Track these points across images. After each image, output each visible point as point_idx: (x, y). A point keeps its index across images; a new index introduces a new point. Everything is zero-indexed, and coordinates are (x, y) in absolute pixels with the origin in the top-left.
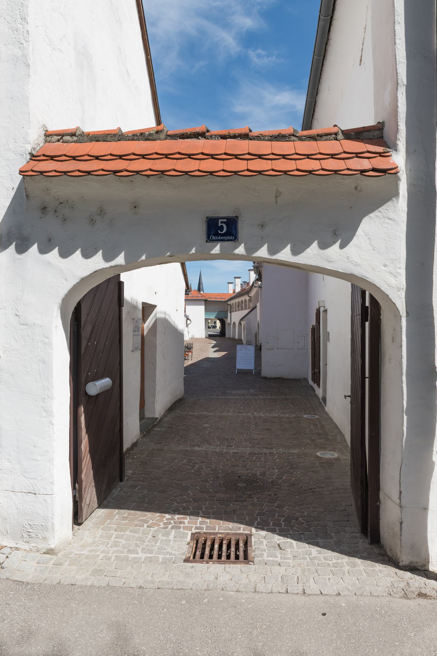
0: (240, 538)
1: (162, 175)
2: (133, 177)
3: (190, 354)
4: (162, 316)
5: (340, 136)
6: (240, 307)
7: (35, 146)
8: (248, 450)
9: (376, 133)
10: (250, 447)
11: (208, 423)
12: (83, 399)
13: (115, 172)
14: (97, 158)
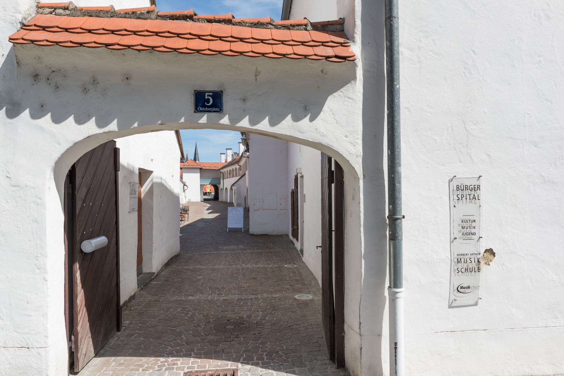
0: (228, 373)
1: (152, 51)
2: (125, 50)
3: (187, 215)
4: (159, 181)
5: (309, 27)
6: (231, 174)
7: (26, 16)
8: (237, 297)
9: (338, 27)
10: (238, 294)
11: (201, 275)
12: (78, 256)
13: (107, 45)
14: (90, 31)
